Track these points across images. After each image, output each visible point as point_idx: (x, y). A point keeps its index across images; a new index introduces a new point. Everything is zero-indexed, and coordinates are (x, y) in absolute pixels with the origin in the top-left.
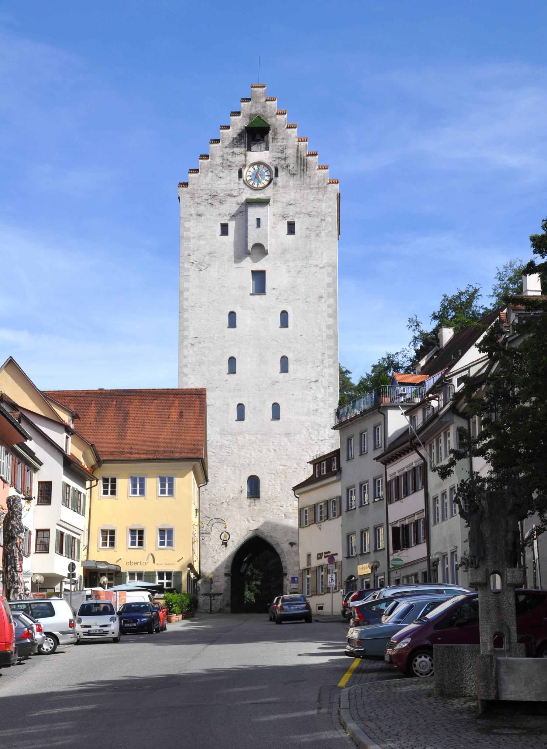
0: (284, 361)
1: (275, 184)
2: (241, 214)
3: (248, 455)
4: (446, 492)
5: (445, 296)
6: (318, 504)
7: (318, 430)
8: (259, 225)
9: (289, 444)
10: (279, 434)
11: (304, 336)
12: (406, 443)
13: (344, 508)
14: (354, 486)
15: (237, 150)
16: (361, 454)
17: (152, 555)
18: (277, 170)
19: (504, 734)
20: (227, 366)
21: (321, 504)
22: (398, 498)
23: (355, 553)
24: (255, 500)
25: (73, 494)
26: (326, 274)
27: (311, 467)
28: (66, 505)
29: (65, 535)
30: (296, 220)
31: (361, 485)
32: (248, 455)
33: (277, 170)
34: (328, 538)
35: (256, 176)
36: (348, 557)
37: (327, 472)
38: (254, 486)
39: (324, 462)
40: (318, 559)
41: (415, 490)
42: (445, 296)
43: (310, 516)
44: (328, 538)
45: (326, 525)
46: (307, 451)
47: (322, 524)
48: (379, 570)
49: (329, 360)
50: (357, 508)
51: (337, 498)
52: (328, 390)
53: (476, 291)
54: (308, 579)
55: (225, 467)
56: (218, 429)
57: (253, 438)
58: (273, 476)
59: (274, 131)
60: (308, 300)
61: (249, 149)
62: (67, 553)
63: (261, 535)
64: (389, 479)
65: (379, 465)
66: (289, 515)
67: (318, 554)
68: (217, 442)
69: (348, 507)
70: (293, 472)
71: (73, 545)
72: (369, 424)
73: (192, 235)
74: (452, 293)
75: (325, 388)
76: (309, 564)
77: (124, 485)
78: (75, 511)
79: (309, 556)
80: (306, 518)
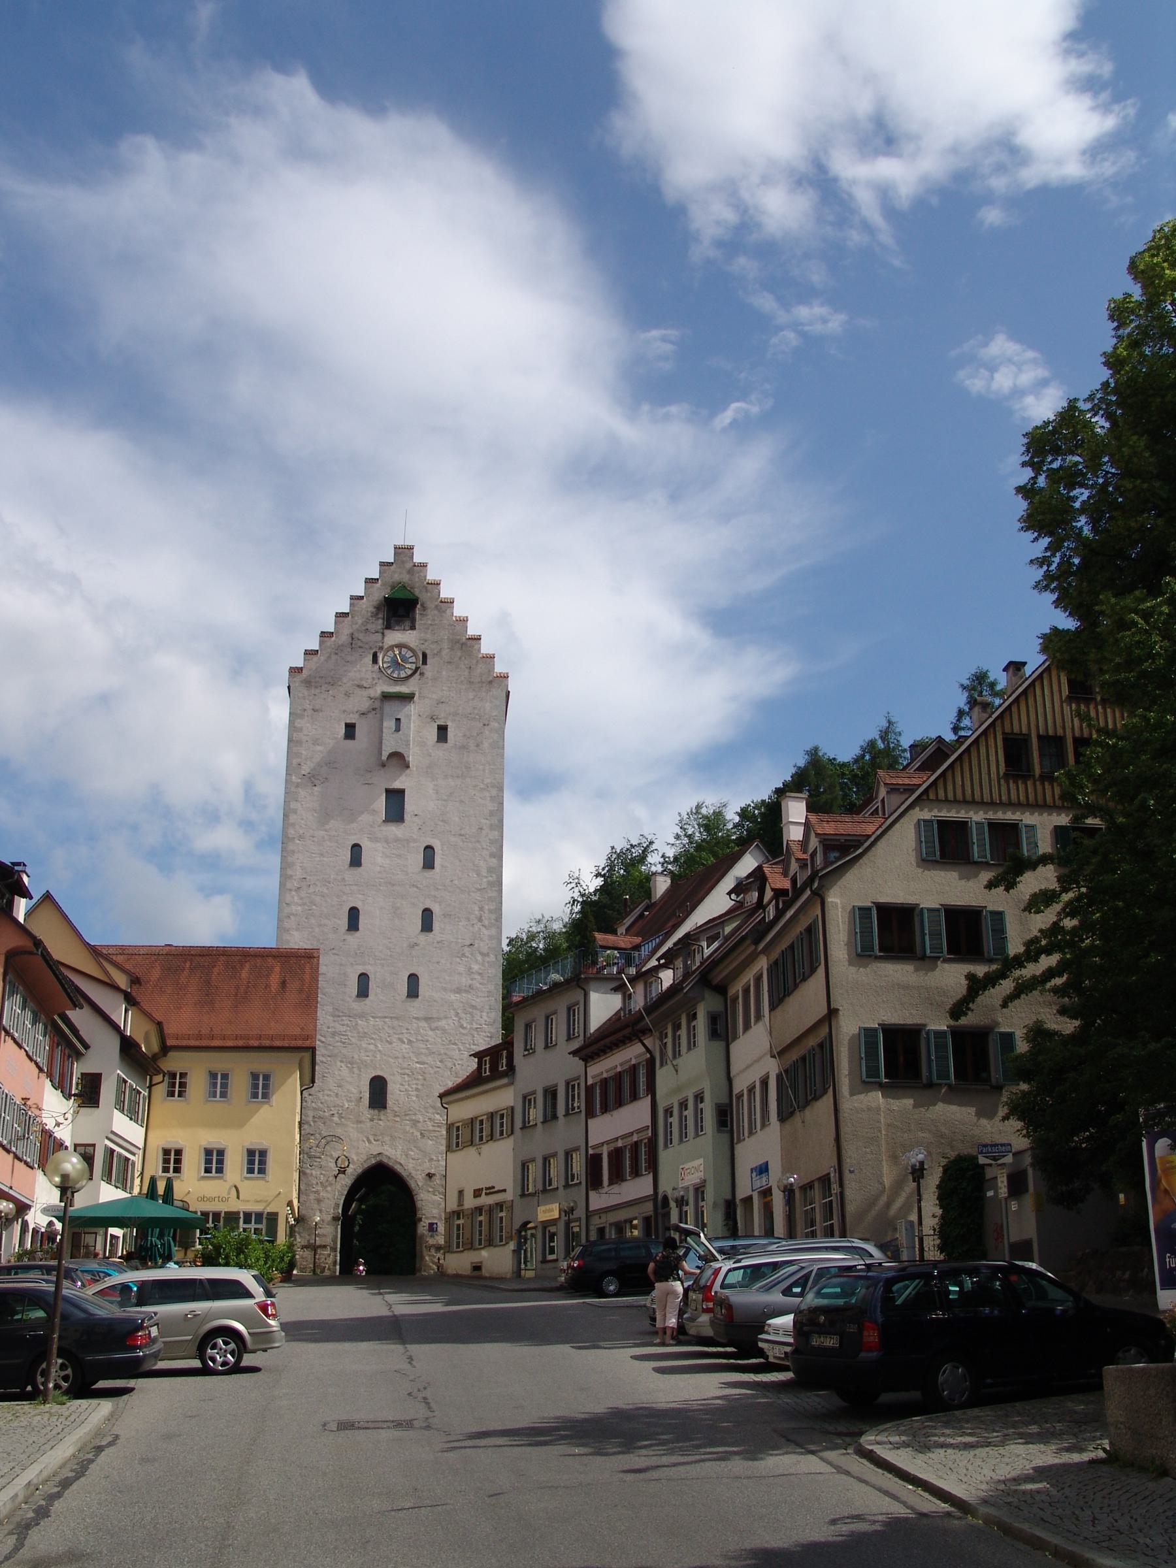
0: (427, 915)
1: (422, 674)
3: (372, 1047)
4: (754, 1087)
5: (613, 848)
7: (471, 1014)
8: (398, 729)
9: (431, 1033)
11: (456, 882)
12: (621, 1031)
13: (518, 1123)
14: (534, 1093)
15: (371, 627)
16: (546, 1047)
18: (425, 656)
19: (950, 1446)
22: (605, 1109)
23: (554, 1185)
25: (131, 1093)
28: (119, 1110)
31: (567, 1083)
32: (372, 1047)
33: (425, 656)
35: (396, 664)
36: (523, 1195)
38: (378, 1092)
40: (475, 1196)
41: (635, 1097)
42: (613, 848)
44: (492, 1166)
45: (489, 1149)
46: (455, 1044)
48: (576, 1214)
50: (539, 1125)
52: (487, 959)
53: (651, 843)
54: (458, 1226)
55: (339, 1064)
56: (330, 1009)
57: (379, 1022)
58: (407, 1078)
59: (422, 605)
61: (388, 627)
62: (117, 1180)
63: (385, 1160)
64: (590, 1082)
65: (576, 1064)
66: (427, 1134)
69: (524, 1122)
72: (560, 1005)
73: (304, 738)
75: (483, 955)
76: (460, 1203)
77: (197, 1084)
79: (461, 1193)
80: (458, 1138)
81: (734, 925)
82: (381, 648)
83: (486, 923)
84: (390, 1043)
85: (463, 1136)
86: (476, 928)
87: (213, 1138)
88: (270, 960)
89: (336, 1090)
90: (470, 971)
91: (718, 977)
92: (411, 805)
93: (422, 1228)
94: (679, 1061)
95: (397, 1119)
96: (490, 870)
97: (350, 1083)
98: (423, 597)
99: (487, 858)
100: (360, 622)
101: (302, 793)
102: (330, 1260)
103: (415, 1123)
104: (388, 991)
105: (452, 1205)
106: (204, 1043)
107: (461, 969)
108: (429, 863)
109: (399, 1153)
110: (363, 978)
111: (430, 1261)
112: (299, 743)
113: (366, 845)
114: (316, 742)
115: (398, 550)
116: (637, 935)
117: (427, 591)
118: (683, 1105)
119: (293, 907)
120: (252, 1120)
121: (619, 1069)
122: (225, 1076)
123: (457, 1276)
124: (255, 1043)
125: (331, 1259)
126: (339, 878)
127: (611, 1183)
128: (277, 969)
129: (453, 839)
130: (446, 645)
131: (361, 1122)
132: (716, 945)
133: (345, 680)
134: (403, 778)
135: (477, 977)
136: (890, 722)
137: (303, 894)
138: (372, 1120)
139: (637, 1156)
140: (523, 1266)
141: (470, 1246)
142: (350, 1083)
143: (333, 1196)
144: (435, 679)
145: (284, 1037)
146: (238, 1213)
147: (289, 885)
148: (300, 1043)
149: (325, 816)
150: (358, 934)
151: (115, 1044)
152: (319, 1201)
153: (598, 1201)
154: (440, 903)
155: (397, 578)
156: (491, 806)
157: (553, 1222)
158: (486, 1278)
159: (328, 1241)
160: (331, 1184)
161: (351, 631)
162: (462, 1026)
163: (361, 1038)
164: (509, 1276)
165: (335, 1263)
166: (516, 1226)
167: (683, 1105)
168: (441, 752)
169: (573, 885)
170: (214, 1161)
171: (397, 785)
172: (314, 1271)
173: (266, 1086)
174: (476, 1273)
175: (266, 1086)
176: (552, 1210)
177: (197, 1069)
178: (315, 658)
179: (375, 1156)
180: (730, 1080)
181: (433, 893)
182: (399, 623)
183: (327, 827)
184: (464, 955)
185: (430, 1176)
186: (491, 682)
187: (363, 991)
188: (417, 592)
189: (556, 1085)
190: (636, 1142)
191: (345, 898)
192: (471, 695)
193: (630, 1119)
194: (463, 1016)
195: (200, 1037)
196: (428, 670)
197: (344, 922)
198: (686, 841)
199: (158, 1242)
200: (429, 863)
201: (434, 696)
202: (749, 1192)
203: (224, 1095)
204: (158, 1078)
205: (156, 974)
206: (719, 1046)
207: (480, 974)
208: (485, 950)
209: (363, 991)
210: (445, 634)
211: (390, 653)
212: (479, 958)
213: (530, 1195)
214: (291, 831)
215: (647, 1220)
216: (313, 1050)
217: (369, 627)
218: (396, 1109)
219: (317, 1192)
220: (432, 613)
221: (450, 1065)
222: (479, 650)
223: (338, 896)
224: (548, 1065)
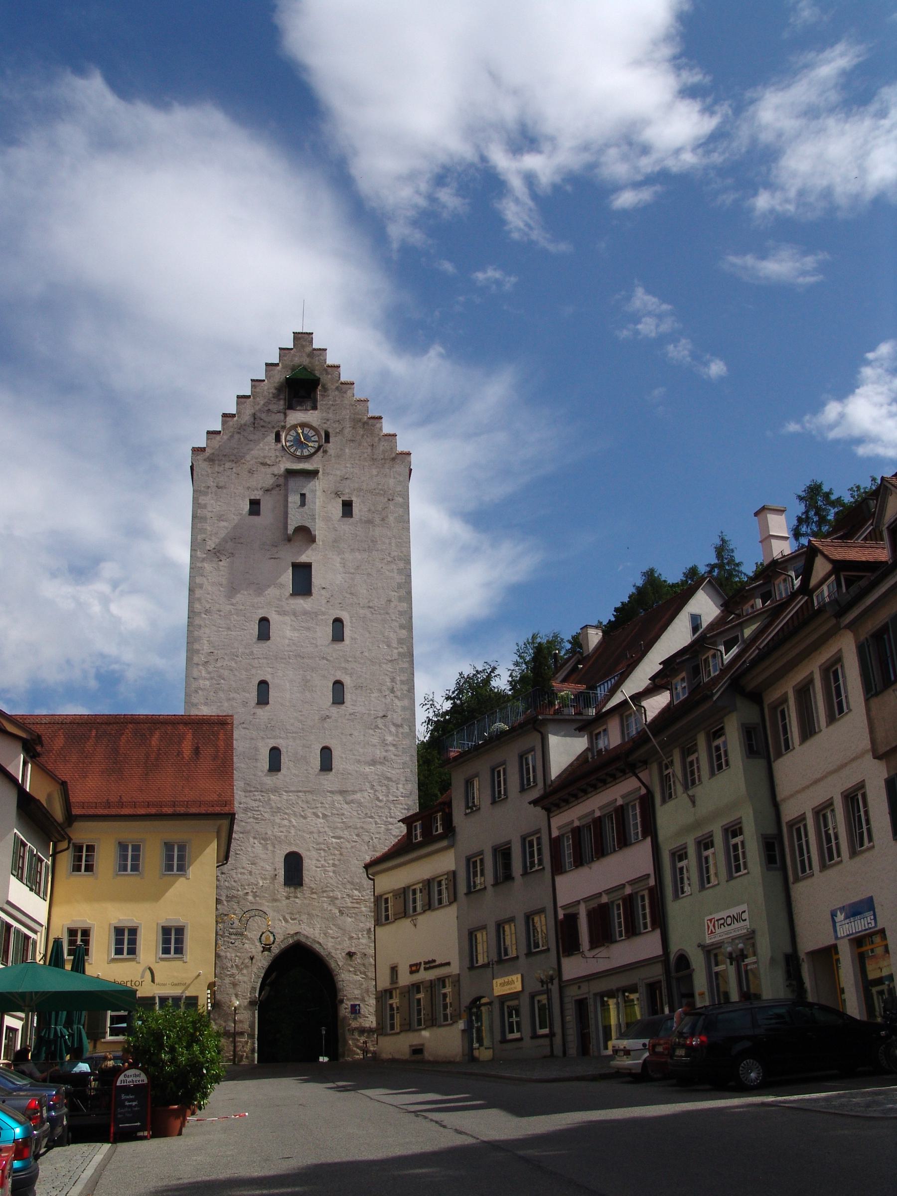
1: (325, 452)
2: (278, 489)
3: (286, 822)
6: (409, 887)
8: (303, 504)
9: (346, 806)
10: (331, 792)
11: (366, 654)
13: (462, 888)
14: (481, 853)
16: (494, 802)
17: (150, 969)
20: (254, 694)
21: (386, 896)
22: (580, 861)
24: (295, 888)
26: (396, 571)
27: (404, 829)
29: (13, 930)
30: (354, 499)
31: (524, 839)
32: (286, 822)
33: (327, 435)
34: (435, 937)
35: (298, 443)
36: (472, 968)
37: (423, 834)
38: (294, 868)
39: (418, 824)
40: (412, 972)
42: (461, 674)
43: (390, 909)
44: (435, 937)
45: (422, 919)
46: (371, 817)
47: (420, 918)
49: (403, 686)
50: (489, 888)
51: (447, 874)
52: (401, 730)
53: (494, 669)
55: (252, 840)
57: (293, 797)
58: (323, 854)
60: (371, 604)
61: (290, 407)
63: (303, 940)
64: (555, 833)
65: (539, 811)
67: (411, 966)
68: (240, 803)
69: (469, 886)
70: (352, 847)
71: (25, 950)
72: (510, 755)
73: (209, 515)
74: (468, 671)
75: (397, 726)
78: (31, 890)
79: (394, 970)
81: (754, 627)
82: (284, 427)
83: (399, 694)
84: (305, 818)
85: (390, 909)
86: (388, 700)
87: (121, 914)
88: (181, 727)
89: (249, 867)
90: (384, 743)
91: (752, 682)
92: (317, 579)
93: (344, 1010)
94: (698, 791)
95: (315, 896)
96: (400, 642)
97: (264, 860)
98: (324, 379)
99: (397, 629)
100: (262, 402)
101: (207, 566)
102: (248, 1048)
103: (333, 899)
104: (300, 765)
105: (384, 982)
106: (113, 811)
107: (375, 740)
108: (338, 635)
109: (317, 932)
110: (275, 753)
111: (355, 1048)
112: (204, 519)
113: (274, 618)
114: (221, 518)
115: (298, 336)
116: (579, 682)
117: (327, 373)
118: (705, 843)
119: (201, 682)
120: (167, 894)
121: (598, 814)
122: (136, 848)
123: (393, 1061)
124: (169, 810)
125: (249, 1046)
126: (247, 651)
127: (594, 945)
128: (189, 736)
129: (362, 611)
130: (348, 424)
131: (276, 900)
132: (735, 650)
133: (248, 457)
134: (309, 552)
135: (392, 748)
136: (723, 540)
137: (211, 668)
138: (288, 898)
139: (641, 907)
140: (476, 1045)
141: (408, 1027)
142: (264, 860)
143: (246, 984)
144: (338, 456)
145: (200, 804)
146: (153, 998)
147: (196, 659)
148: (218, 809)
149: (232, 590)
150: (268, 707)
151: (10, 800)
152: (234, 985)
153: (573, 968)
154: (351, 675)
155: (297, 360)
156: (399, 579)
157: (515, 996)
158: (429, 1062)
159: (246, 1026)
160: (247, 967)
161: (253, 411)
162: (378, 799)
163: (274, 813)
164: (458, 1059)
165: (253, 1051)
166: (466, 1000)
167: (705, 843)
168: (346, 527)
169: (428, 706)
170: (125, 940)
171: (303, 559)
172: (234, 1060)
173: (181, 858)
174: (418, 1057)
175: (181, 858)
176: (513, 982)
177: (105, 843)
178: (218, 437)
179: (292, 936)
180: (776, 805)
181: (343, 665)
182: (300, 403)
183: (234, 601)
184: (377, 727)
185: (350, 955)
186: (393, 459)
187: (275, 764)
188: (317, 373)
189: (509, 842)
190: (630, 895)
191: (253, 671)
192: (375, 472)
193: (628, 865)
194: (378, 788)
195: (108, 804)
196: (331, 447)
197: (253, 695)
198: (524, 666)
199: (65, 1031)
200: (338, 635)
201: (338, 473)
202: (827, 940)
203: (135, 868)
204: (63, 845)
205: (59, 742)
206: (761, 763)
207: (394, 745)
208: (399, 722)
209: (275, 764)
210: (346, 414)
211: (293, 433)
212: (393, 729)
213: (483, 966)
214: (197, 606)
215: (653, 988)
216: (231, 817)
217: (271, 407)
218: (313, 886)
219: (232, 975)
220: (333, 394)
221: (367, 839)
222: (381, 429)
223: (247, 670)
224: (494, 821)
